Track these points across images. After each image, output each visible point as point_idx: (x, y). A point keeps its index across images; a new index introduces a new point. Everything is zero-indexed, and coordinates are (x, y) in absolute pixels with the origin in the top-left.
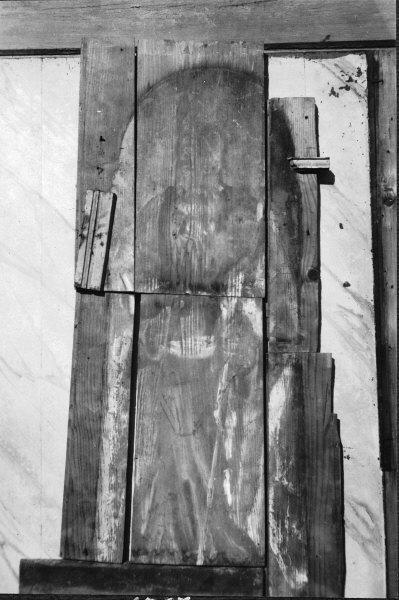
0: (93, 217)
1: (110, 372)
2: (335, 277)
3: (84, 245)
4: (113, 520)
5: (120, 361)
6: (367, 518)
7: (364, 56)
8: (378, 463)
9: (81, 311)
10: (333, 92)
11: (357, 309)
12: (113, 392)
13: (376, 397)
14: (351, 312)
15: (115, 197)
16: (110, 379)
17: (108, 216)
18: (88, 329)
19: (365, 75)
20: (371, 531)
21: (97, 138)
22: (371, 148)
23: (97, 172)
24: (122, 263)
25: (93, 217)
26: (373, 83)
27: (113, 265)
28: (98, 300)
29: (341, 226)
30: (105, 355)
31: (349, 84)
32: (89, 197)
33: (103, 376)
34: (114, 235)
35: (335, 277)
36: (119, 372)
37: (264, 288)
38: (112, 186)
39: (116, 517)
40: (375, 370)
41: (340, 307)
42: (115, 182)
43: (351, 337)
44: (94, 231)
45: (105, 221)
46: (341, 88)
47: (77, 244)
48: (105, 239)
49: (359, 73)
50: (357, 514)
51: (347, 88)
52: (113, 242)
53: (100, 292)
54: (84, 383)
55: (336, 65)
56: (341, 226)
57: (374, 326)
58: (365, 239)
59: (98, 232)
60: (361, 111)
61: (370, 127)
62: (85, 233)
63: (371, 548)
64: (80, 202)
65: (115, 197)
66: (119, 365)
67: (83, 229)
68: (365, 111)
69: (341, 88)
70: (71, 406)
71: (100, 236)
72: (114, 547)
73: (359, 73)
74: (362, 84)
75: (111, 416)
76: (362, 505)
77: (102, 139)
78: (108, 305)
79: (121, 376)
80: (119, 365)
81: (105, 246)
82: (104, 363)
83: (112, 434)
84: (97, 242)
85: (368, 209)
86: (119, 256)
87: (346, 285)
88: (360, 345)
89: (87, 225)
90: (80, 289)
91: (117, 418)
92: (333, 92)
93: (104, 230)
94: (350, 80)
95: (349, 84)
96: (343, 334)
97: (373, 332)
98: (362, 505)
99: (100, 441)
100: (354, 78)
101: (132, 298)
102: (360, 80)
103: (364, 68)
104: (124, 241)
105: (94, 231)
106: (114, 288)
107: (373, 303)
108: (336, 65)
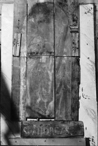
0: (16, 39)
1: (21, 75)
2: (86, 56)
3: (14, 46)
4: (23, 111)
5: (24, 73)
6: (93, 113)
7: (93, 4)
8: (96, 100)
9: (13, 62)
10: (85, 13)
11: (91, 64)
12: (22, 81)
13: (96, 85)
14: (90, 64)
15: (21, 34)
16: (21, 77)
17: (20, 39)
18: (16, 66)
19: (93, 9)
20: (95, 116)
21: (18, 20)
22: (94, 26)
23: (18, 28)
24: (24, 50)
25: (16, 39)
26: (95, 11)
27: (21, 51)
28: (17, 59)
29: (87, 44)
30: (20, 72)
31: (89, 11)
32: (15, 34)
33: (19, 77)
34: (22, 43)
35: (86, 56)
36: (23, 76)
37: (59, 57)
38: (21, 32)
39: (24, 110)
40: (95, 78)
41: (87, 63)
42: (22, 31)
43: (89, 70)
44: (17, 42)
45: (19, 40)
46: (87, 12)
47: (13, 45)
48: (19, 44)
49: (92, 8)
50: (91, 112)
51: (89, 12)
52: (21, 45)
53: (19, 57)
54: (15, 79)
55: (86, 6)
56: (87, 44)
57: (95, 68)
58: (93, 47)
59: (18, 43)
60: (92, 17)
61: (94, 21)
62: (15, 43)
63: (94, 120)
64: (14, 35)
65: (21, 34)
66: (23, 74)
67: (14, 42)
68: (93, 17)
69: (87, 12)
70: (12, 84)
71: (18, 44)
72: (24, 117)
73: (92, 8)
74: (92, 11)
75: (22, 86)
76: (92, 110)
77: (19, 21)
78: (20, 59)
79: (24, 77)
80: (23, 74)
81: (19, 46)
82: (20, 74)
83: (22, 90)
84: (18, 45)
85: (93, 40)
86: (23, 48)
87: (89, 58)
88: (92, 72)
89: (15, 41)
90: (13, 56)
91: (23, 87)
92: (85, 13)
93: (19, 42)
94: (90, 10)
95: (89, 11)
96: (87, 70)
97: (95, 69)
98: (92, 110)
99: (19, 92)
100: (90, 10)
101: (26, 58)
102: (92, 10)
103: (93, 7)
104: (24, 45)
105: (17, 42)
106: (22, 56)
107: (95, 62)
108: (86, 6)
